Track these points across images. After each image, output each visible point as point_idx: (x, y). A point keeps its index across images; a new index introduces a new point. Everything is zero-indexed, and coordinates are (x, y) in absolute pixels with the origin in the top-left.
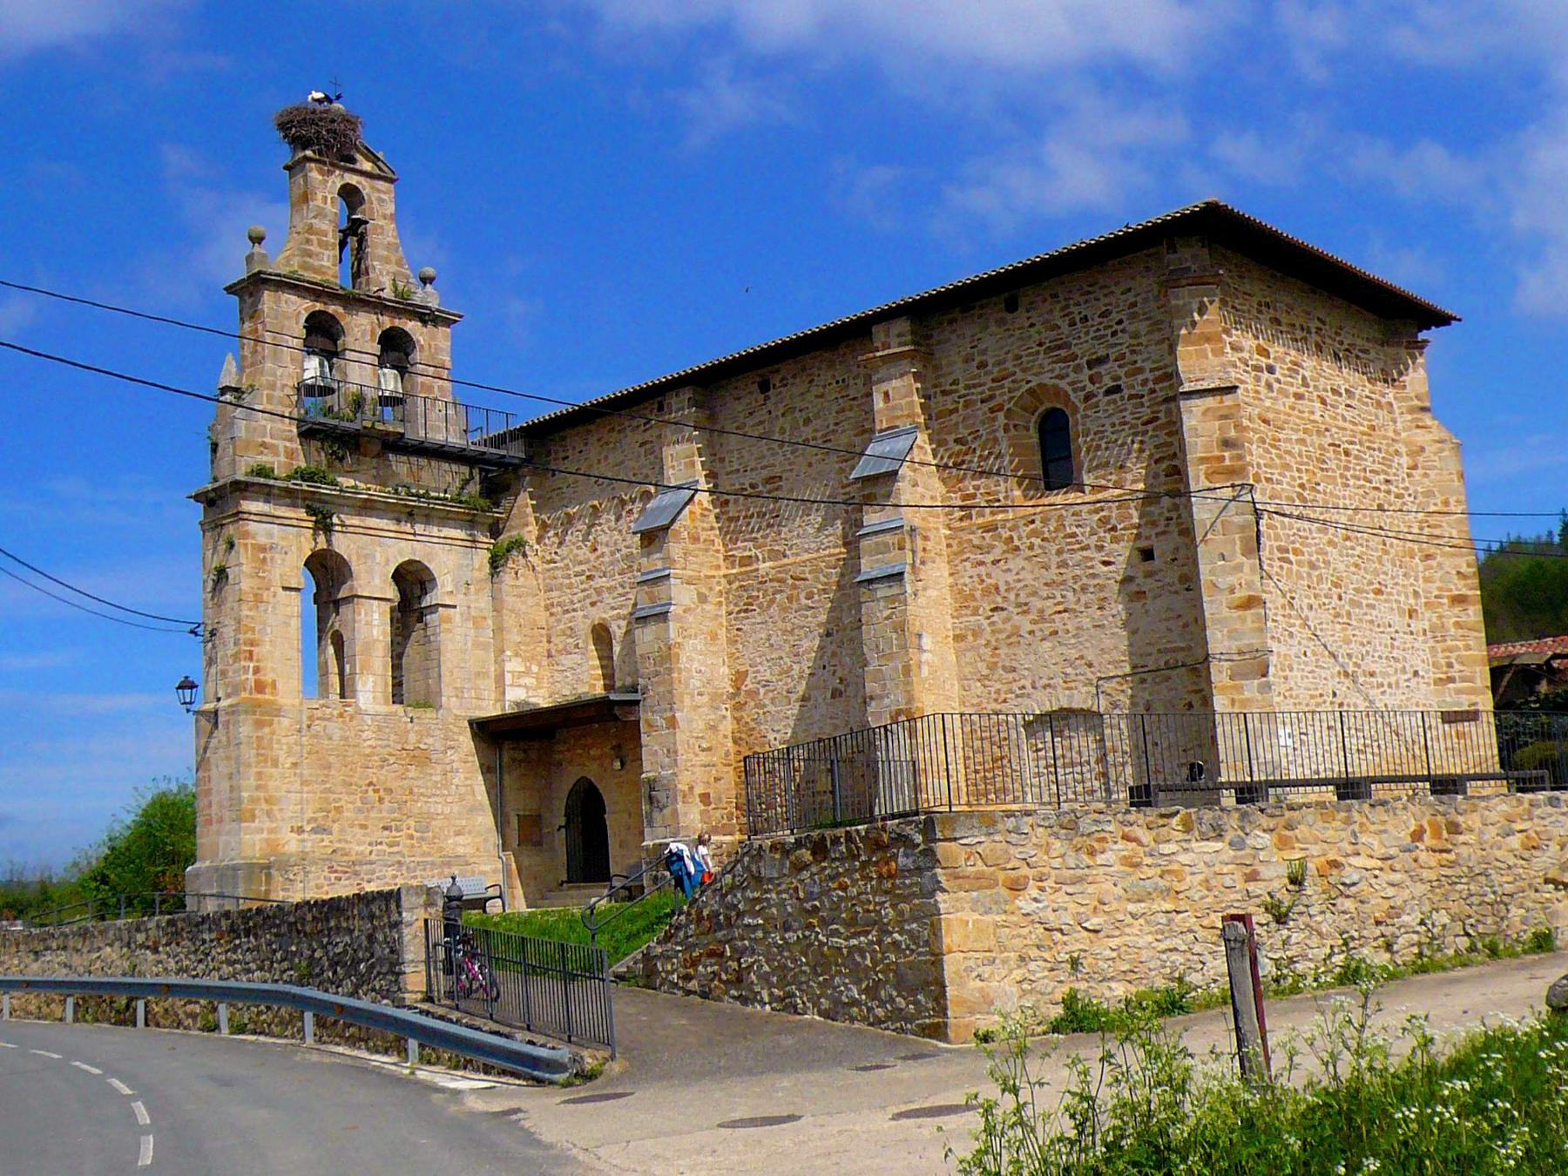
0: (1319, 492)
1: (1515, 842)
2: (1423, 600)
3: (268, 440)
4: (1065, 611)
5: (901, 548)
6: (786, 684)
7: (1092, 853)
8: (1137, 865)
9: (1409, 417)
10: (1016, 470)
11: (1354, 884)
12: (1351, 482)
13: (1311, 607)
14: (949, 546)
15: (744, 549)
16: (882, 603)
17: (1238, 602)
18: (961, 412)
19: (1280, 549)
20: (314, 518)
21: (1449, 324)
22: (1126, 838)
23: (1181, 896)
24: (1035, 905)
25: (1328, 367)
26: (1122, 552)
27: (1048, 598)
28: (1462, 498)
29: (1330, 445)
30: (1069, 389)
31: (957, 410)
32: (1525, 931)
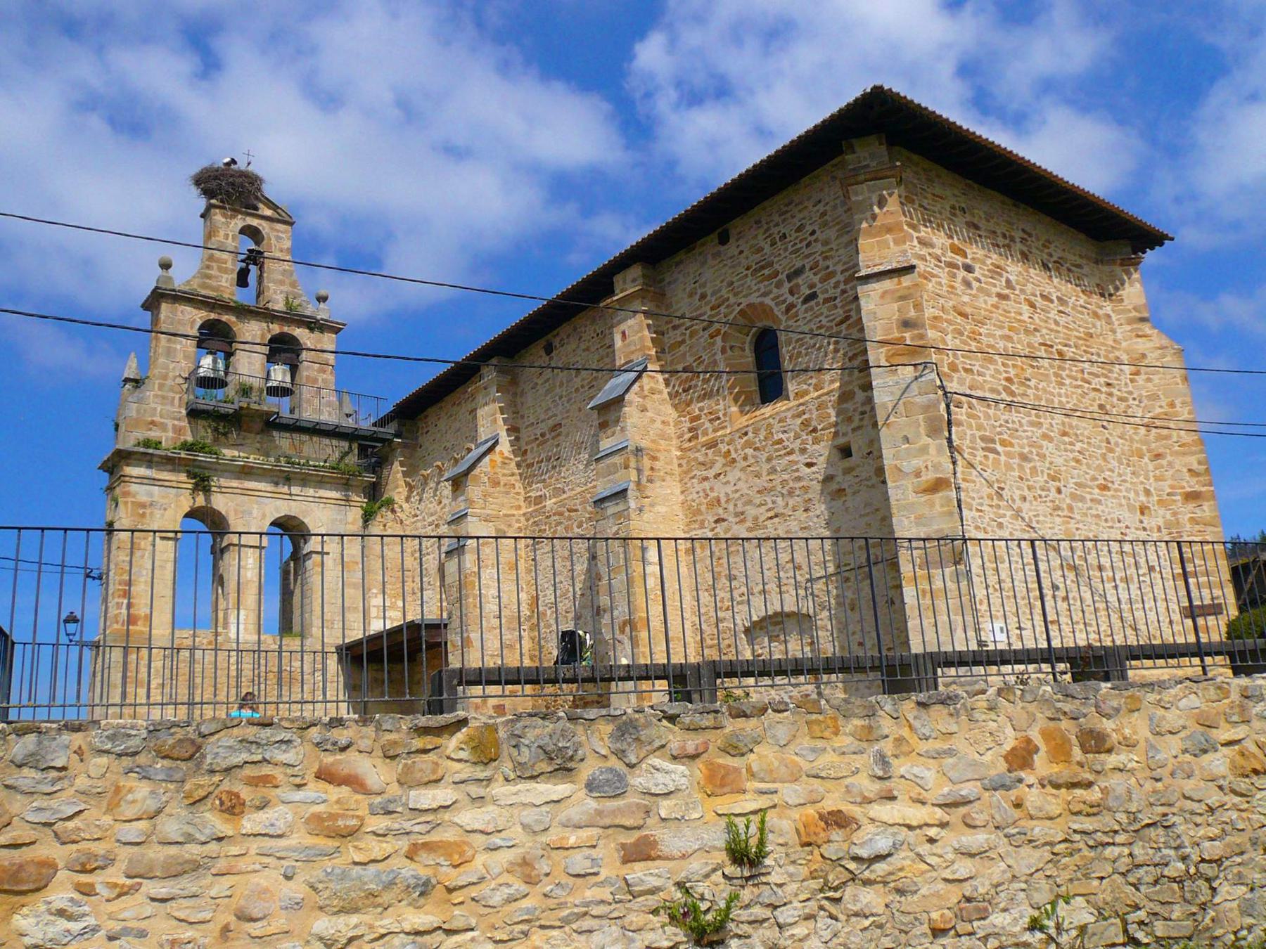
0: (1029, 387)
1: (1218, 762)
2: (1156, 498)
3: (157, 419)
4: (776, 516)
5: (626, 467)
6: (565, 605)
7: (233, 808)
8: (349, 834)
9: (1128, 328)
10: (732, 388)
11: (880, 858)
12: (1068, 381)
13: (1024, 499)
14: (680, 465)
15: (537, 490)
16: (611, 520)
17: (924, 486)
18: (688, 342)
19: (983, 439)
20: (193, 481)
21: (1161, 244)
22: (326, 776)
23: (457, 897)
24: (63, 924)
25: (1037, 275)
26: (822, 451)
27: (760, 506)
28: (1188, 399)
29: (1041, 344)
30: (772, 304)
31: (683, 342)
32: (1250, 929)
